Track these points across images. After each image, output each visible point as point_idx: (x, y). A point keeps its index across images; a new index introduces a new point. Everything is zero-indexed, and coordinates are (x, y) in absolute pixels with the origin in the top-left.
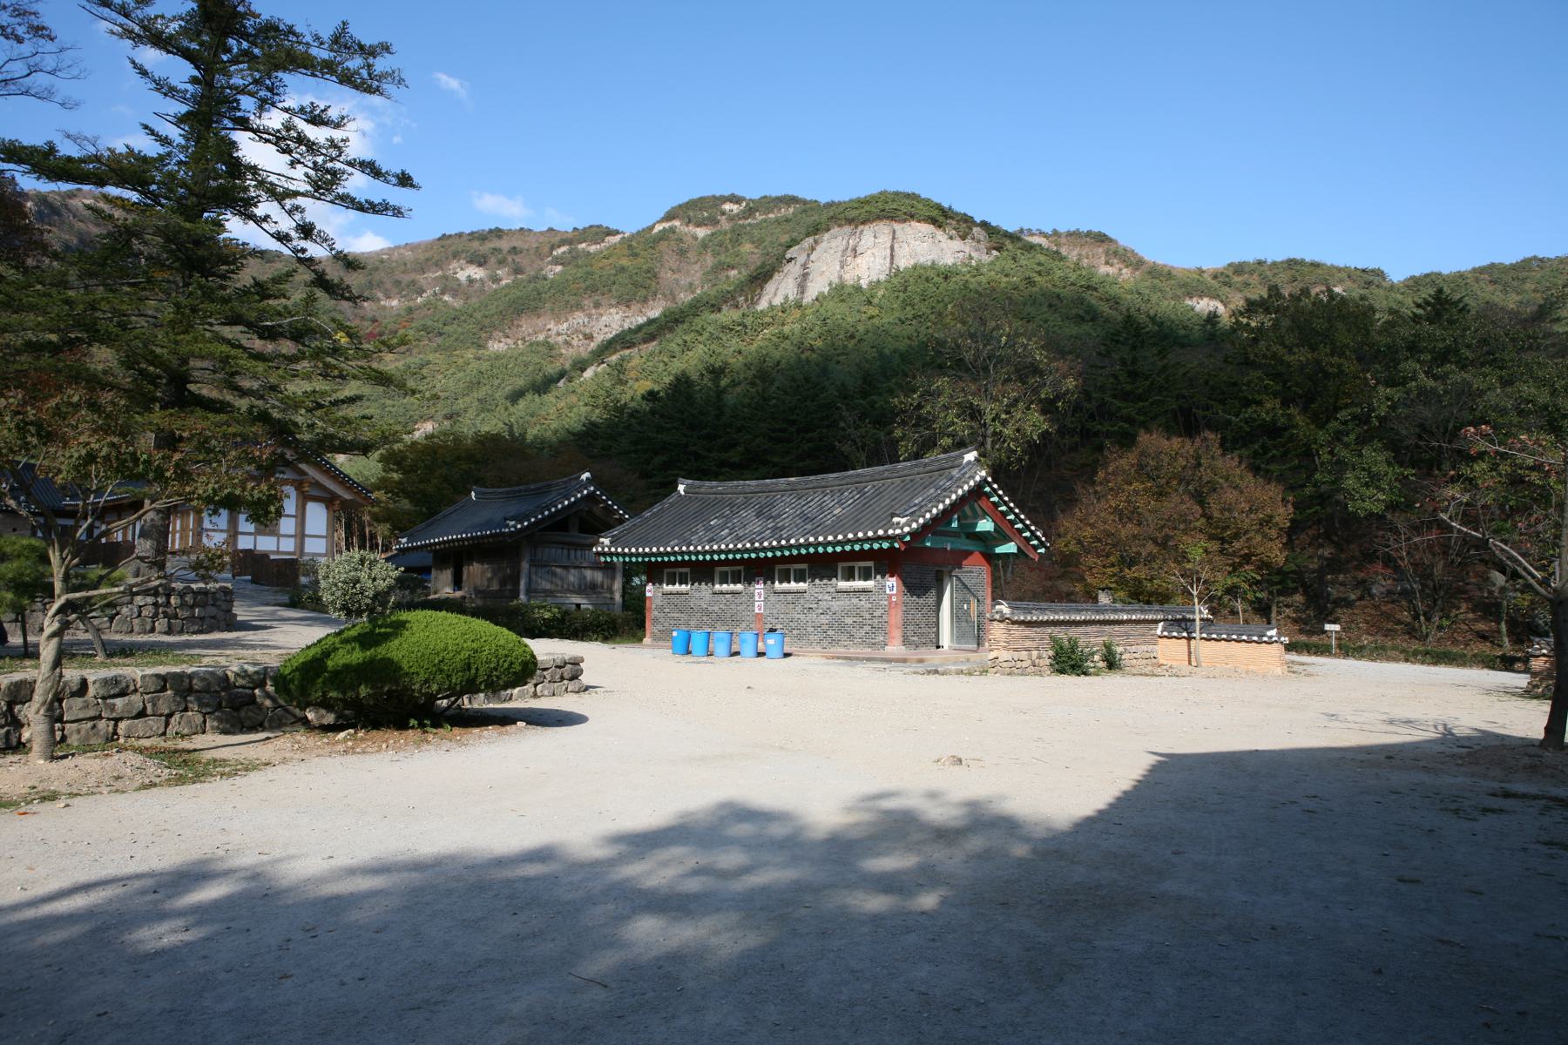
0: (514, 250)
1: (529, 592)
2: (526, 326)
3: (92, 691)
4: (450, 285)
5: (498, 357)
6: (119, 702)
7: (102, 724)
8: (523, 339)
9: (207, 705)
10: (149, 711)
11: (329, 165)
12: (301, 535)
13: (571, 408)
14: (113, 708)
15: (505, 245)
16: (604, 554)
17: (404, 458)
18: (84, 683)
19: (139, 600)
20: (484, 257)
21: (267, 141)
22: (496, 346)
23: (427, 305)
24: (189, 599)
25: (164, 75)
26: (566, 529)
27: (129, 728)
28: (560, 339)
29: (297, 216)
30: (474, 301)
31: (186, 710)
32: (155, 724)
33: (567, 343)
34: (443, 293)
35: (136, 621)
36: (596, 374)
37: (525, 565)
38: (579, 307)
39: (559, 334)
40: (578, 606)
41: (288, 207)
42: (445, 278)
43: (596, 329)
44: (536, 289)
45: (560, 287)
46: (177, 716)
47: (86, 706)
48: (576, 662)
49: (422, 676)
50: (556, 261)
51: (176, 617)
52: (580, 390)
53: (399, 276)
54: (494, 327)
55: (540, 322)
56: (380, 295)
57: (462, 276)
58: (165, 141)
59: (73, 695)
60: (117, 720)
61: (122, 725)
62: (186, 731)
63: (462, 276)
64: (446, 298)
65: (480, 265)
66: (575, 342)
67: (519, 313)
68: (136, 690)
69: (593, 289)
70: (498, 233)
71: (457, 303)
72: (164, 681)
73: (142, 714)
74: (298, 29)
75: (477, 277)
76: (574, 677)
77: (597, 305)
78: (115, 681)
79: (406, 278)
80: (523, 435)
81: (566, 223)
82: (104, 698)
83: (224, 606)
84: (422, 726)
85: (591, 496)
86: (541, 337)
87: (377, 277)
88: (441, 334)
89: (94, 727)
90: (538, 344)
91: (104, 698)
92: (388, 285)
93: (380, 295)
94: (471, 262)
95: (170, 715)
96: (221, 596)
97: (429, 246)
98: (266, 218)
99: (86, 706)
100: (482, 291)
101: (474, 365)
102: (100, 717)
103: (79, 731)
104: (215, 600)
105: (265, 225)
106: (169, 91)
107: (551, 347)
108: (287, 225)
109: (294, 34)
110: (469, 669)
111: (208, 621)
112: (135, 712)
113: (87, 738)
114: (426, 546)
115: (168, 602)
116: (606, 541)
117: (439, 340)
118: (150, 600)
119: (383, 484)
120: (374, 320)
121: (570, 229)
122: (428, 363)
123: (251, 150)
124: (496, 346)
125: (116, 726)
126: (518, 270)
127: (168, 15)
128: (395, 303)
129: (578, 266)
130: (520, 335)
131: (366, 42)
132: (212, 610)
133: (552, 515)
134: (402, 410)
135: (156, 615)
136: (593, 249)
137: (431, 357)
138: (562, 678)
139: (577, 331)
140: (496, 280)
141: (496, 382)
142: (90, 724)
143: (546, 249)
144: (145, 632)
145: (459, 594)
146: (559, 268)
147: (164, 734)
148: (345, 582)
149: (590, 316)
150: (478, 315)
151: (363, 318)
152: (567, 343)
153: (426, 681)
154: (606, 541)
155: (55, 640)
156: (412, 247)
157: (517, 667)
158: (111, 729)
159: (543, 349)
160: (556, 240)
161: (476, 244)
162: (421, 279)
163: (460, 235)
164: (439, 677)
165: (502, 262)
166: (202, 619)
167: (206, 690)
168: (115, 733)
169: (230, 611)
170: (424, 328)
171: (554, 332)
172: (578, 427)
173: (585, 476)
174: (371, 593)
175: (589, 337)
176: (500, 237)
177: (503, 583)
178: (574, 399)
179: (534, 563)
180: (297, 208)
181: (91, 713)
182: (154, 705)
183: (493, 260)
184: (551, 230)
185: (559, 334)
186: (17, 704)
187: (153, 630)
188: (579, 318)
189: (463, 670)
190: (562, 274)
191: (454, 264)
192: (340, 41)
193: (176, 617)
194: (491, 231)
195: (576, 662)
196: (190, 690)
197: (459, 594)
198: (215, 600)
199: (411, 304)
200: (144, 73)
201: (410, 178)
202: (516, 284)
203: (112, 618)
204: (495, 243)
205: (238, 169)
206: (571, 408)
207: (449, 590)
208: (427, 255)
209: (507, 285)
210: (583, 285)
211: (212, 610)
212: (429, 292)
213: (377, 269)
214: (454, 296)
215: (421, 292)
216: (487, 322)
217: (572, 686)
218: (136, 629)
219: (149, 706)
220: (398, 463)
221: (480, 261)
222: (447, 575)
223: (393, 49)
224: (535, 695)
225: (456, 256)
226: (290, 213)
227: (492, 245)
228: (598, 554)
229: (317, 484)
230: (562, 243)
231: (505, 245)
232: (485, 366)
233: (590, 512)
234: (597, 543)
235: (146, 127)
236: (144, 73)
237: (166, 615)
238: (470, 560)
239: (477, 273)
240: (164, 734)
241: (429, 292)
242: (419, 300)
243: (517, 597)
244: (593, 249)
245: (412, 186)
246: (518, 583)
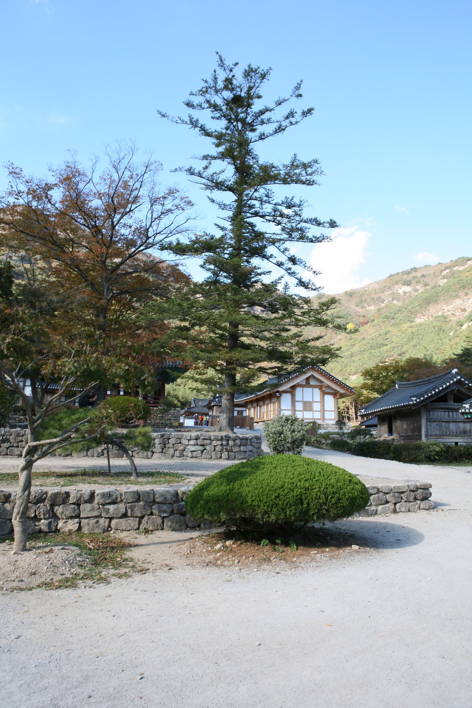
0: (423, 276)
1: (427, 436)
2: (434, 310)
3: (97, 500)
4: (395, 296)
5: (420, 325)
6: (111, 507)
7: (102, 521)
8: (432, 316)
9: (165, 512)
10: (129, 514)
11: (299, 226)
12: (323, 411)
13: (457, 344)
14: (108, 511)
15: (418, 274)
16: (466, 413)
17: (373, 373)
18: (92, 495)
19: (214, 443)
20: (410, 281)
21: (270, 221)
22: (419, 320)
23: (387, 306)
24: (238, 442)
25: (221, 200)
26: (446, 401)
27: (117, 524)
28: (450, 313)
29: (287, 253)
30: (407, 302)
31: (152, 514)
32: (133, 522)
33: (453, 315)
34: (393, 300)
35: (213, 453)
36: (469, 326)
37: (424, 422)
38: (457, 297)
39: (449, 311)
40: (456, 443)
41: (282, 250)
42: (393, 293)
43: (467, 306)
44: (435, 292)
45: (447, 289)
46: (146, 518)
47: (93, 510)
48: (426, 488)
49: (263, 508)
50: (444, 277)
51: (232, 451)
52: (460, 335)
53: (373, 296)
54: (417, 312)
55: (439, 307)
56: (366, 305)
57: (400, 292)
58: (223, 229)
59: (86, 502)
60: (111, 519)
61: (114, 522)
62: (151, 528)
63: (400, 292)
64: (394, 302)
65: (408, 285)
66: (457, 314)
67: (429, 303)
68: (122, 501)
69: (464, 287)
70: (415, 269)
71: (400, 304)
72: (138, 497)
73: (125, 516)
74: (275, 165)
75: (408, 291)
76: (425, 498)
77: (466, 294)
78: (109, 495)
79: (376, 296)
80: (431, 359)
81: (447, 260)
82: (103, 505)
83: (257, 446)
84: (273, 542)
85: (459, 382)
86: (440, 314)
87: (364, 298)
88: (393, 318)
89: (97, 522)
90: (439, 317)
91: (102, 505)
92: (369, 301)
93: (366, 305)
94: (404, 284)
95: (142, 517)
96: (254, 440)
97: (385, 281)
98: (271, 256)
99: (93, 510)
100: (410, 297)
101: (410, 330)
102: (100, 516)
103: (88, 524)
104: (251, 442)
105: (271, 259)
106: (223, 206)
107: (445, 318)
108: (283, 258)
109: (273, 167)
110: (302, 504)
111: (248, 453)
112: (120, 514)
113: (93, 529)
114: (375, 412)
115: (228, 444)
116: (467, 406)
117: (393, 321)
118: (219, 443)
119: (365, 386)
120: (364, 317)
121: (449, 262)
122: (389, 332)
123: (261, 225)
124: (419, 320)
125: (110, 522)
126: (426, 285)
127: (218, 172)
128: (372, 308)
129: (454, 278)
130: (430, 314)
131: (306, 161)
132: (250, 448)
133: (436, 394)
134: (379, 354)
135: (222, 450)
136: (461, 268)
137: (390, 329)
138: (415, 499)
139: (458, 308)
140: (416, 291)
141: (420, 337)
142: (95, 520)
143: (438, 273)
144: (217, 459)
145: (391, 437)
146: (445, 280)
147: (138, 529)
148: (274, 433)
149: (463, 300)
150: (409, 308)
151: (359, 316)
152: (453, 315)
153: (266, 512)
154: (467, 406)
155: (25, 472)
156: (378, 283)
157: (345, 502)
158: (107, 524)
159: (442, 319)
160: (443, 268)
161: (405, 276)
162: (382, 296)
163: (398, 274)
164: (275, 510)
165: (418, 282)
166: (245, 452)
167: (163, 503)
168: (109, 526)
169: (260, 448)
170: (386, 317)
171: (446, 310)
172: (460, 352)
173: (455, 371)
174: (290, 440)
175: (464, 310)
176: (416, 271)
177: (413, 431)
178: (458, 339)
179: (428, 420)
180: (286, 249)
181: (95, 513)
182: (132, 511)
183: (414, 282)
184: (440, 263)
185: (449, 311)
186: (55, 505)
187: (221, 457)
188: (458, 302)
189: (295, 504)
190: (446, 283)
191: (397, 287)
192: (293, 166)
193: (232, 451)
194: (412, 269)
195: (426, 488)
196: (154, 502)
197: (391, 437)
198: (251, 442)
199: (380, 307)
200: (213, 201)
201: (335, 222)
202: (426, 291)
203: (202, 451)
204: (414, 274)
205: (259, 236)
206: (457, 344)
207: (386, 435)
208: (384, 285)
209: (422, 292)
210: (458, 286)
211: (250, 448)
212: (387, 301)
213: (364, 294)
214: (398, 301)
215: (383, 301)
216: (414, 310)
217: (423, 504)
218: (213, 457)
219: (129, 511)
220: (371, 376)
221: (408, 283)
222: (385, 428)
223: (319, 162)
224: (395, 511)
225: (397, 283)
226: (283, 252)
227: (413, 276)
228: (463, 414)
229: (328, 387)
230: (446, 268)
231: (418, 274)
232: (414, 330)
233: (459, 391)
234: (462, 407)
235: (216, 225)
236: (213, 201)
237: (227, 450)
238: (396, 419)
239: (407, 289)
240: (138, 529)
241: (387, 301)
242: (383, 305)
243: (420, 438)
244: (461, 268)
245: (337, 226)
246: (420, 431)
